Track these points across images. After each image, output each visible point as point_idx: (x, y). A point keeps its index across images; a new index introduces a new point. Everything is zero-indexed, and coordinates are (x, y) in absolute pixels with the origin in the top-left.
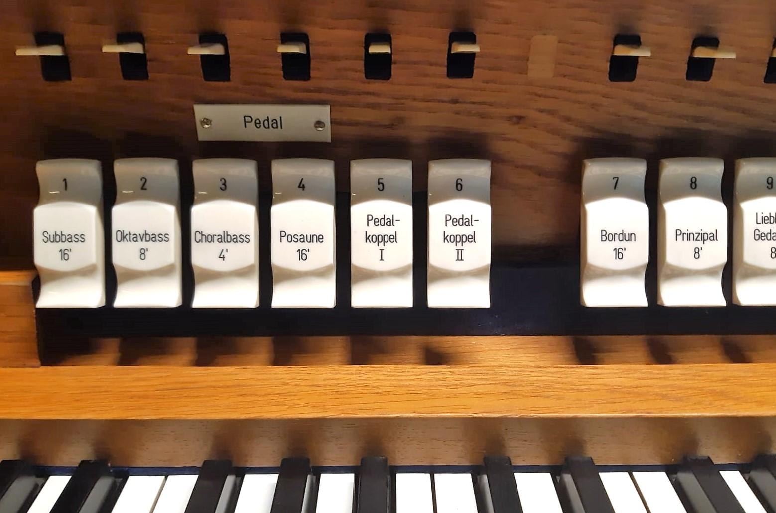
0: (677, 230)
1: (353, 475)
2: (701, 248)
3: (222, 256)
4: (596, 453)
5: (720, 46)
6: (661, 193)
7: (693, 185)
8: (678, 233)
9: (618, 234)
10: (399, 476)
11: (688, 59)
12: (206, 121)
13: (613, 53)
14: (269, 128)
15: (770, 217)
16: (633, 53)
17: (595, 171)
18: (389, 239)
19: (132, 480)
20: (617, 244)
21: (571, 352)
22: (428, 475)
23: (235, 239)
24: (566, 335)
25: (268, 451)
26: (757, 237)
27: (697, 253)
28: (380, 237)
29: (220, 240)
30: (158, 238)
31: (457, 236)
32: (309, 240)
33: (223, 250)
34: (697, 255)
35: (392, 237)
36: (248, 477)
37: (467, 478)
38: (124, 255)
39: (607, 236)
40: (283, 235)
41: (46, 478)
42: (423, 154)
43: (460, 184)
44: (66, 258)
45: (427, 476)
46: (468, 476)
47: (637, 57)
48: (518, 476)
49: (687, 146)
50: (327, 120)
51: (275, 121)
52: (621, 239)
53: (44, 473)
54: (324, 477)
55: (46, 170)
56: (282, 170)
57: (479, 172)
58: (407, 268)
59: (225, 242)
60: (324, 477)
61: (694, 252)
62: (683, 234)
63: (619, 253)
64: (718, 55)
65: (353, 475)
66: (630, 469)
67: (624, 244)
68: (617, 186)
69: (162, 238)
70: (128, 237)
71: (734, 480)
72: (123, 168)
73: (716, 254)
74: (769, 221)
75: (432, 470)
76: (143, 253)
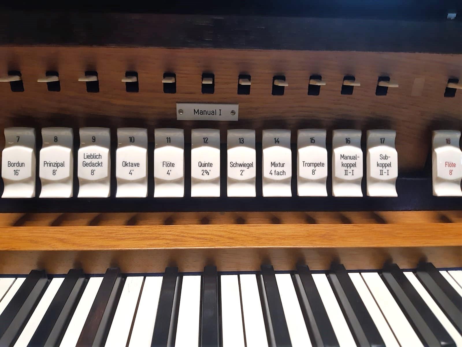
0: (44, 162)
1: (200, 276)
2: (244, 170)
4: (347, 264)
5: (390, 80)
6: (298, 145)
7: (56, 140)
8: (45, 163)
9: (307, 163)
10: (223, 277)
12: (181, 111)
13: (309, 83)
14: (210, 114)
15: (91, 155)
17: (439, 136)
18: (388, 165)
19: (92, 279)
20: (15, 168)
21: (197, 220)
22: (237, 276)
24: (434, 210)
25: (102, 267)
26: (84, 165)
27: (54, 172)
28: (384, 165)
31: (315, 163)
32: (282, 166)
33: (131, 170)
34: (313, 173)
35: (354, 164)
37: (254, 276)
38: (45, 173)
39: (11, 164)
41: (52, 279)
42: (367, 127)
43: (349, 140)
44: (17, 174)
47: (353, 86)
48: (277, 276)
49: (346, 124)
51: (201, 111)
52: (17, 166)
53: (51, 277)
54: (185, 278)
55: (9, 133)
56: (196, 134)
57: (391, 135)
58: (181, 179)
60: (185, 278)
62: (48, 163)
63: (16, 172)
64: (390, 86)
65: (200, 276)
66: (360, 271)
67: (19, 168)
68: (19, 140)
69: (322, 165)
70: (128, 165)
71: (410, 276)
72: (46, 133)
73: (323, 172)
74: (90, 157)
75: (238, 273)
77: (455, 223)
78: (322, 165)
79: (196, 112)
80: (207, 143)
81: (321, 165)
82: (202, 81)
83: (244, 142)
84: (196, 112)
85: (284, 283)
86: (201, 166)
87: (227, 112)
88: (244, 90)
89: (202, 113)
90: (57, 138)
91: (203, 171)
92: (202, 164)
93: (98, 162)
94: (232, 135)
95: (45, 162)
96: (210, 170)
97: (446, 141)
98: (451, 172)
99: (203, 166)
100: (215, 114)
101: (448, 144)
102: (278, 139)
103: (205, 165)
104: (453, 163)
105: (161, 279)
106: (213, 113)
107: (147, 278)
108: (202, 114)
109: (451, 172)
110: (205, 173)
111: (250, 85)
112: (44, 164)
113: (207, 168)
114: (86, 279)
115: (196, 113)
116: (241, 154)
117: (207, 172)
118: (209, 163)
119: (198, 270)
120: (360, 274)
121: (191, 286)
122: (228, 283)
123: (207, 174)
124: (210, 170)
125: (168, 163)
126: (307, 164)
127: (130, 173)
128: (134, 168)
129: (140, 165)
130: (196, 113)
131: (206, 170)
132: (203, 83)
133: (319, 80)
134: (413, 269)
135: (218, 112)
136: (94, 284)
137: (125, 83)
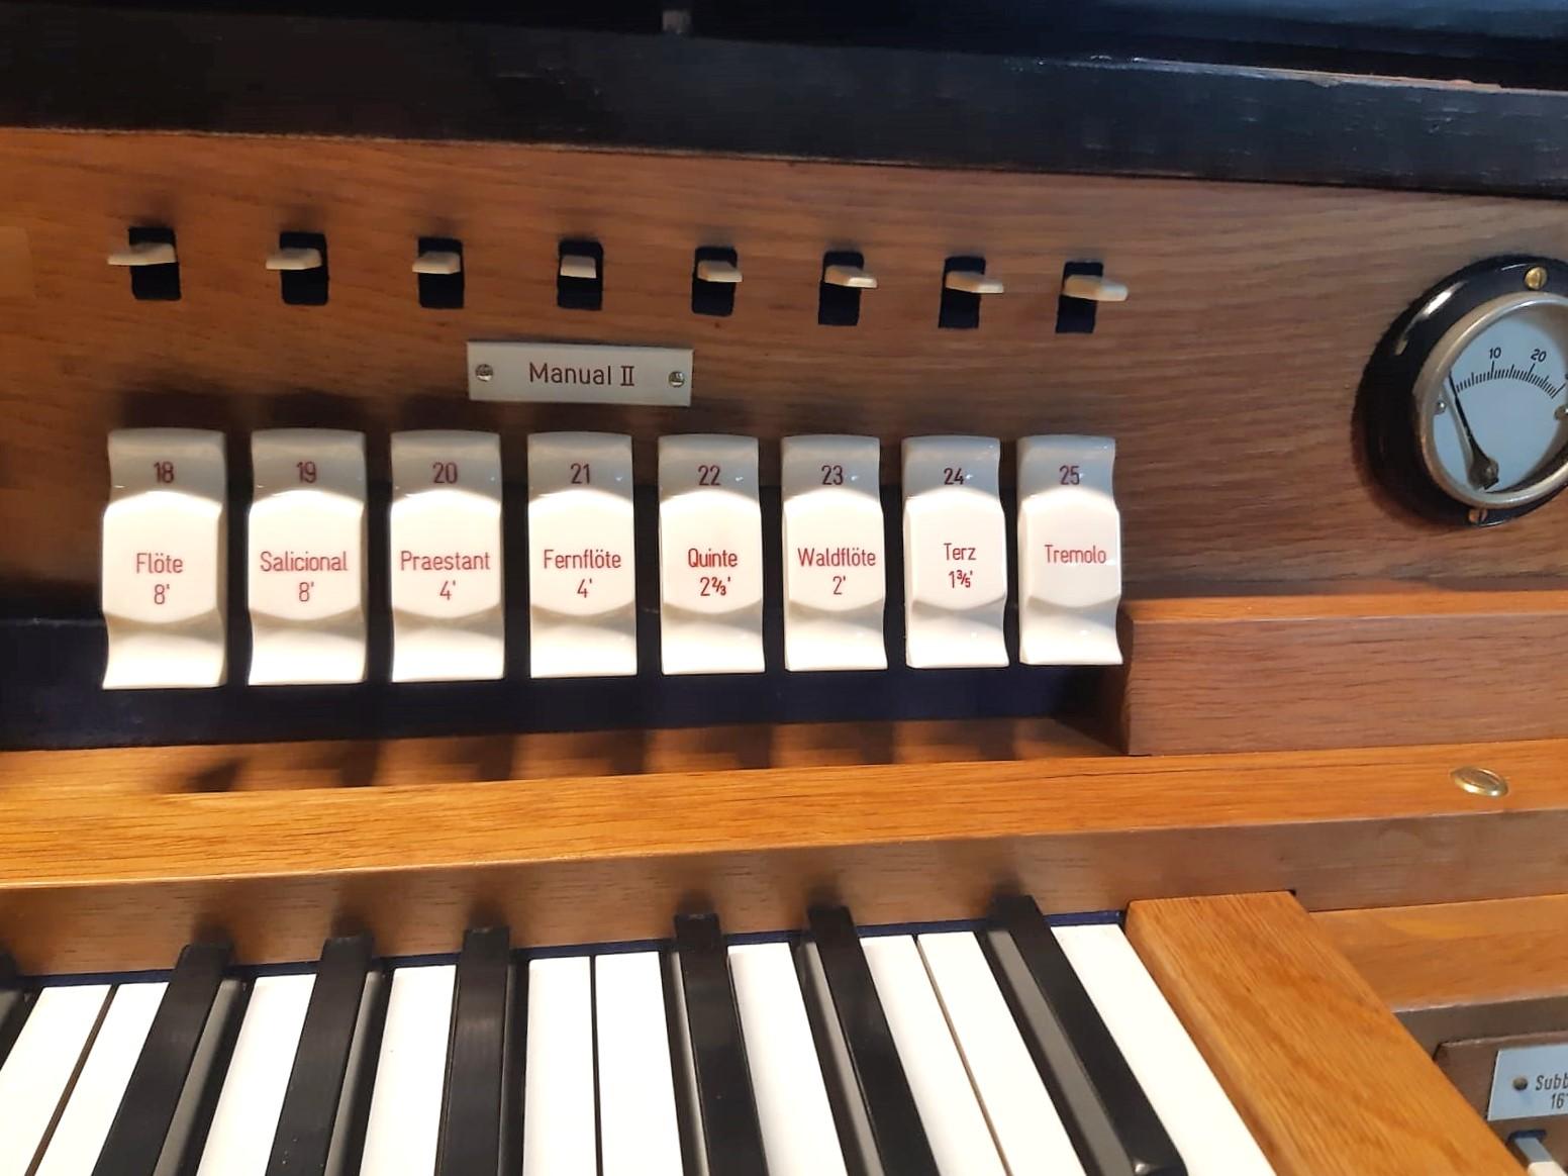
3: (445, 592)
8: (806, 557)
11: (182, 291)
12: (484, 370)
13: (823, 278)
14: (588, 382)
16: (854, 282)
19: (50, 996)
22: (588, 958)
23: (469, 563)
25: (443, 928)
29: (467, 565)
30: (454, 561)
33: (583, 581)
36: (261, 983)
37: (784, 949)
40: (407, 557)
45: (586, 960)
46: (653, 957)
49: (950, 420)
50: (687, 373)
51: (557, 371)
55: (126, 450)
56: (543, 451)
57: (1100, 454)
58: (622, 611)
59: (169, 571)
61: (154, 593)
62: (415, 558)
69: (614, 561)
72: (266, 450)
76: (304, 590)
77: (1020, 759)
78: (614, 561)
79: (539, 372)
80: (718, 484)
81: (866, 559)
82: (560, 266)
83: (459, 478)
84: (539, 372)
85: (766, 979)
86: (696, 565)
87: (659, 373)
88: (713, 300)
89: (561, 378)
90: (172, 468)
91: (705, 581)
92: (699, 557)
93: (1094, 547)
94: (674, 454)
95: (405, 554)
96: (729, 578)
97: (154, 471)
98: (160, 593)
99: (704, 562)
100: (606, 381)
101: (162, 484)
102: (960, 470)
103: (710, 560)
104: (867, 552)
105: (448, 973)
106: (601, 377)
107: (123, 988)
108: (560, 381)
109: (160, 593)
110: (711, 590)
111: (733, 285)
112: (403, 560)
113: (720, 572)
114: (26, 991)
115: (539, 377)
116: (708, 519)
117: (717, 584)
118: (724, 554)
119: (958, 913)
120: (916, 939)
121: (422, 1004)
122: (553, 983)
123: (720, 590)
124: (729, 578)
125: (159, 557)
126: (1058, 555)
127: (582, 590)
128: (455, 574)
129: (184, 566)
130: (539, 377)
131: (715, 579)
132: (565, 272)
133: (973, 274)
134: (973, 921)
135: (617, 376)
136: (280, 1007)
137: (278, 273)
